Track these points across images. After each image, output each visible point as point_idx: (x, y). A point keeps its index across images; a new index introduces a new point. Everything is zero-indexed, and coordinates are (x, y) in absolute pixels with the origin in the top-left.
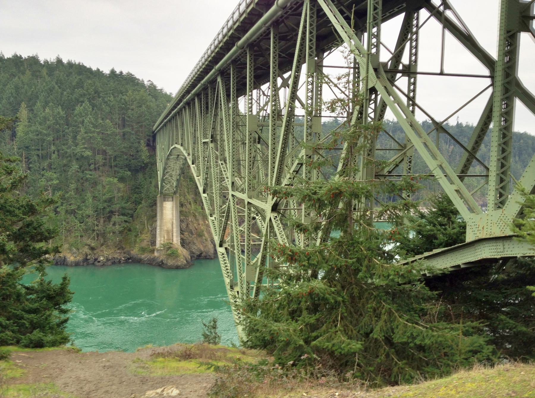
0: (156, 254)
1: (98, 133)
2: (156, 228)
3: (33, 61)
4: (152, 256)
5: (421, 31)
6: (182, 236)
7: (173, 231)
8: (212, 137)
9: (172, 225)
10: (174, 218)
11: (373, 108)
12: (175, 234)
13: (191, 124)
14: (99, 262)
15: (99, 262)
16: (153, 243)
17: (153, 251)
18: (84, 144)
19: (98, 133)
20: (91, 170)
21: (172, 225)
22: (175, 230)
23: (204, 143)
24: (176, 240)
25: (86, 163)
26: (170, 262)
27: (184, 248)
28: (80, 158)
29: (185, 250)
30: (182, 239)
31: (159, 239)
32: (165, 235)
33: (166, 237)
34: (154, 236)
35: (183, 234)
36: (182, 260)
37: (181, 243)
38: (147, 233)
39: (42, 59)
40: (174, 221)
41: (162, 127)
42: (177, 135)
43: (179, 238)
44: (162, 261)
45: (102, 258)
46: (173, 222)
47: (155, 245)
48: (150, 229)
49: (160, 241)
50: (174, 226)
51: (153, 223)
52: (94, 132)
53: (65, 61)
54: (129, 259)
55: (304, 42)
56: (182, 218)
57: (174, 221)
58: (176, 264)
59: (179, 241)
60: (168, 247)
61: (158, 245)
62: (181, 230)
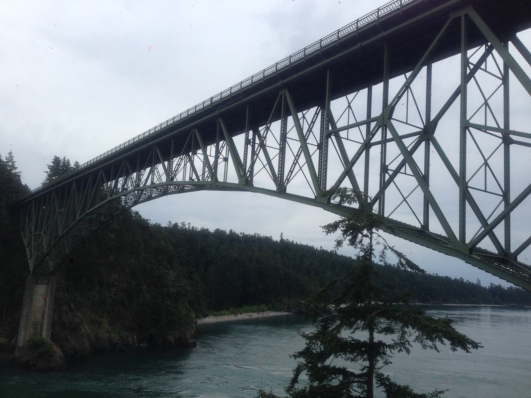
0: (16, 354)
7: (43, 323)
9: (43, 315)
10: (47, 306)
12: (45, 327)
21: (43, 315)
22: (45, 322)
31: (23, 334)
40: (47, 310)
46: (44, 312)
57: (47, 310)
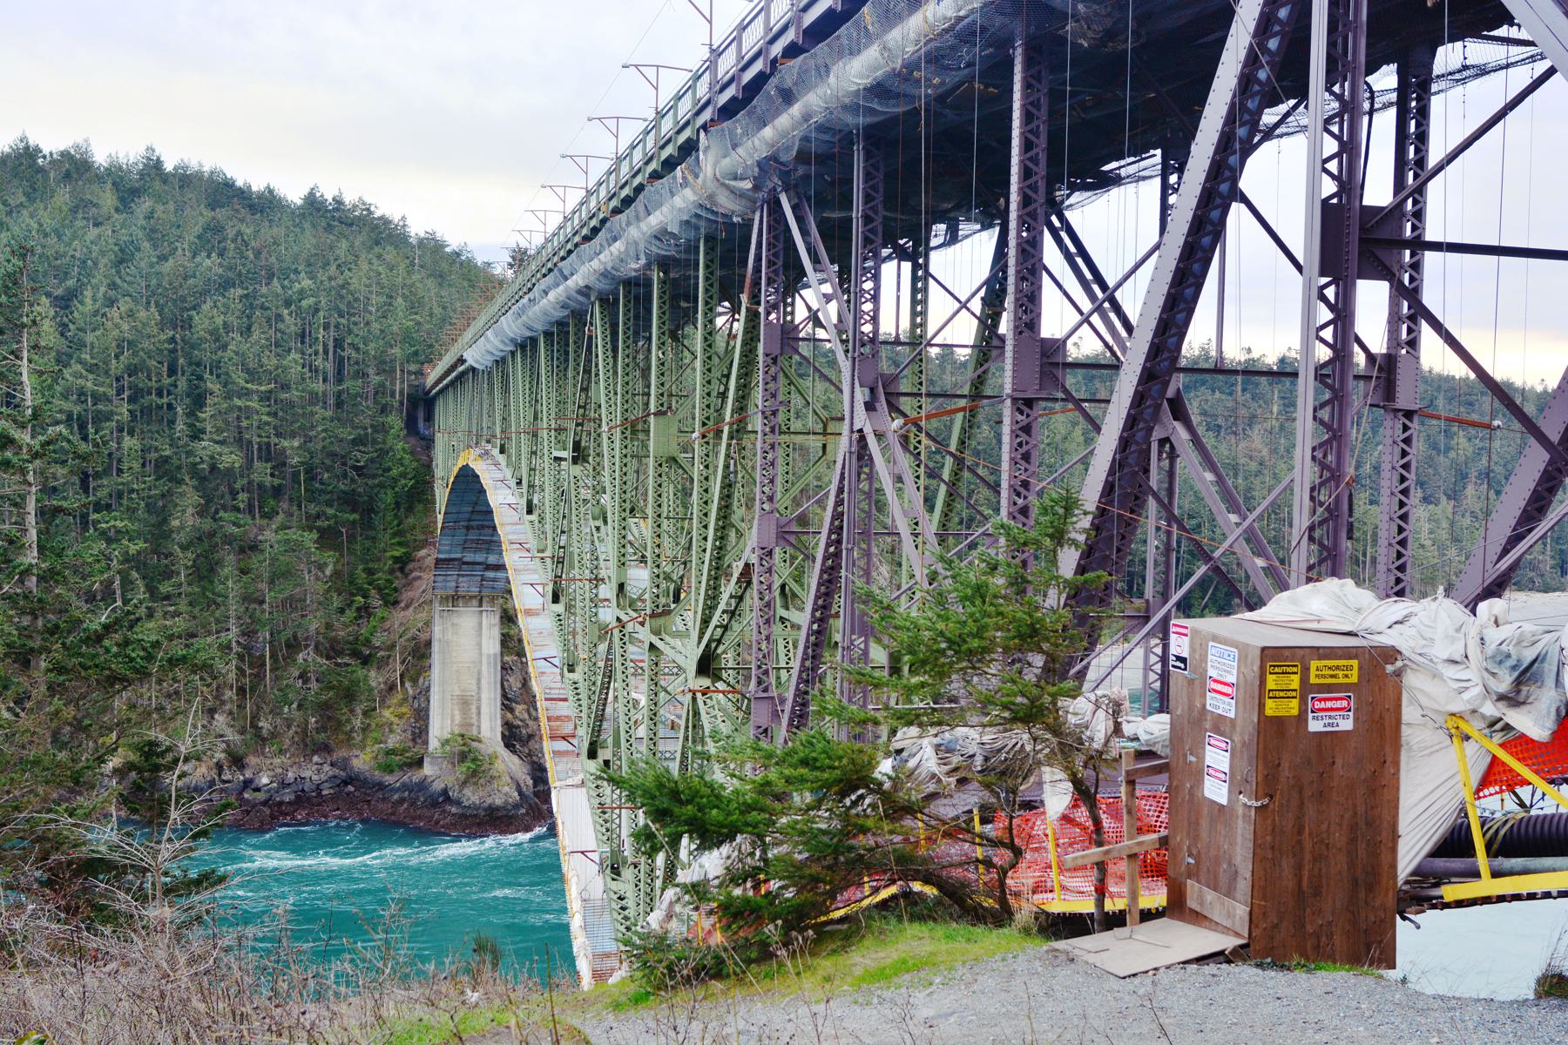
0: (428, 770)
1: (266, 397)
2: (428, 689)
3: (75, 167)
4: (415, 776)
5: (1433, 187)
6: (509, 715)
8: (577, 446)
11: (1160, 653)
12: (485, 709)
13: (528, 379)
14: (258, 790)
15: (258, 790)
16: (420, 733)
17: (419, 763)
18: (219, 431)
19: (266, 397)
20: (238, 510)
21: (479, 680)
22: (485, 696)
23: (556, 459)
24: (490, 729)
25: (223, 489)
26: (471, 796)
27: (514, 752)
28: (210, 478)
29: (515, 759)
30: (507, 725)
32: (457, 712)
33: (458, 718)
34: (422, 715)
35: (512, 710)
36: (506, 789)
37: (503, 736)
38: (401, 705)
39: (100, 158)
41: (452, 383)
42: (492, 405)
43: (499, 722)
44: (445, 792)
45: (265, 780)
46: (479, 673)
47: (426, 743)
48: (411, 692)
49: (440, 727)
50: (484, 682)
51: (419, 675)
52: (247, 394)
53: (169, 167)
54: (346, 783)
55: (754, 327)
56: (507, 658)
57: (484, 668)
58: (489, 801)
59: (499, 729)
60: (465, 752)
61: (434, 744)
62: (505, 696)
